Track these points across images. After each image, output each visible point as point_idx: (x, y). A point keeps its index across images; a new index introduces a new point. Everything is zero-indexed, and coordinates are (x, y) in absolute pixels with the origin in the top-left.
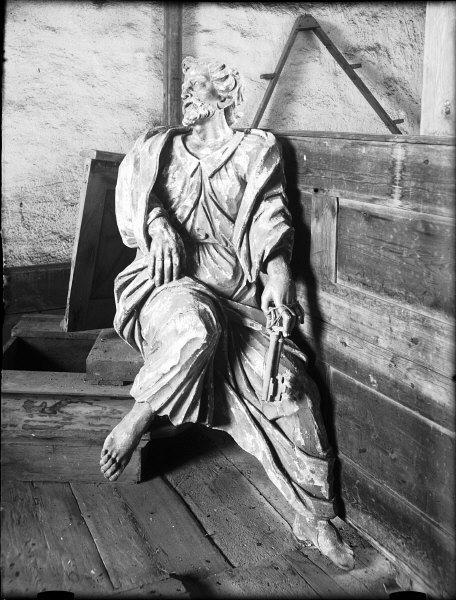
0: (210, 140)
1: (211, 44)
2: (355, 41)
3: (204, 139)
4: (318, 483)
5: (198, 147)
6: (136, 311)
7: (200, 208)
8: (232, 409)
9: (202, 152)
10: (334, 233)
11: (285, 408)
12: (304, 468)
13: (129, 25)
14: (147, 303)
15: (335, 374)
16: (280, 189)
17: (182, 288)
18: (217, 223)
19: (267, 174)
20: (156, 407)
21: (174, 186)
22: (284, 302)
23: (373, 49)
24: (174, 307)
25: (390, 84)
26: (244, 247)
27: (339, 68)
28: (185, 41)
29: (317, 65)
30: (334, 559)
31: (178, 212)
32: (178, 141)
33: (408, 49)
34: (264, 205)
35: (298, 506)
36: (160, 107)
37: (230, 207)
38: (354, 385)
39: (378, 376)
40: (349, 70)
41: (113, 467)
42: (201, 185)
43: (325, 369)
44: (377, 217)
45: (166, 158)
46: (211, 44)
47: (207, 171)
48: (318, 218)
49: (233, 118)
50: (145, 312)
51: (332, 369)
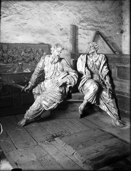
0: (94, 56)
1: (81, 37)
2: (107, 36)
3: (93, 55)
4: (116, 113)
5: (92, 57)
6: (83, 85)
7: (93, 67)
8: (100, 102)
9: (93, 58)
10: (117, 71)
11: (110, 100)
12: (114, 111)
13: (66, 34)
14: (85, 83)
15: (117, 95)
16: (107, 64)
17: (91, 81)
18: (96, 70)
19: (104, 62)
20: (89, 101)
21: (89, 63)
22: (109, 82)
23: (110, 37)
24: (91, 83)
25: (113, 44)
26: (101, 74)
27: (104, 41)
28: (76, 37)
29: (100, 40)
30: (120, 126)
31: (89, 68)
32: (88, 56)
33: (116, 37)
34: (104, 67)
35: (113, 117)
36: (71, 49)
37: (98, 67)
38: (122, 96)
39: (126, 93)
40: (106, 42)
41: (81, 112)
42: (93, 63)
43: (115, 94)
44: (126, 67)
45: (87, 59)
46: (81, 37)
47: (94, 61)
48: (113, 69)
49: (97, 52)
50: (85, 85)
51: (117, 94)
